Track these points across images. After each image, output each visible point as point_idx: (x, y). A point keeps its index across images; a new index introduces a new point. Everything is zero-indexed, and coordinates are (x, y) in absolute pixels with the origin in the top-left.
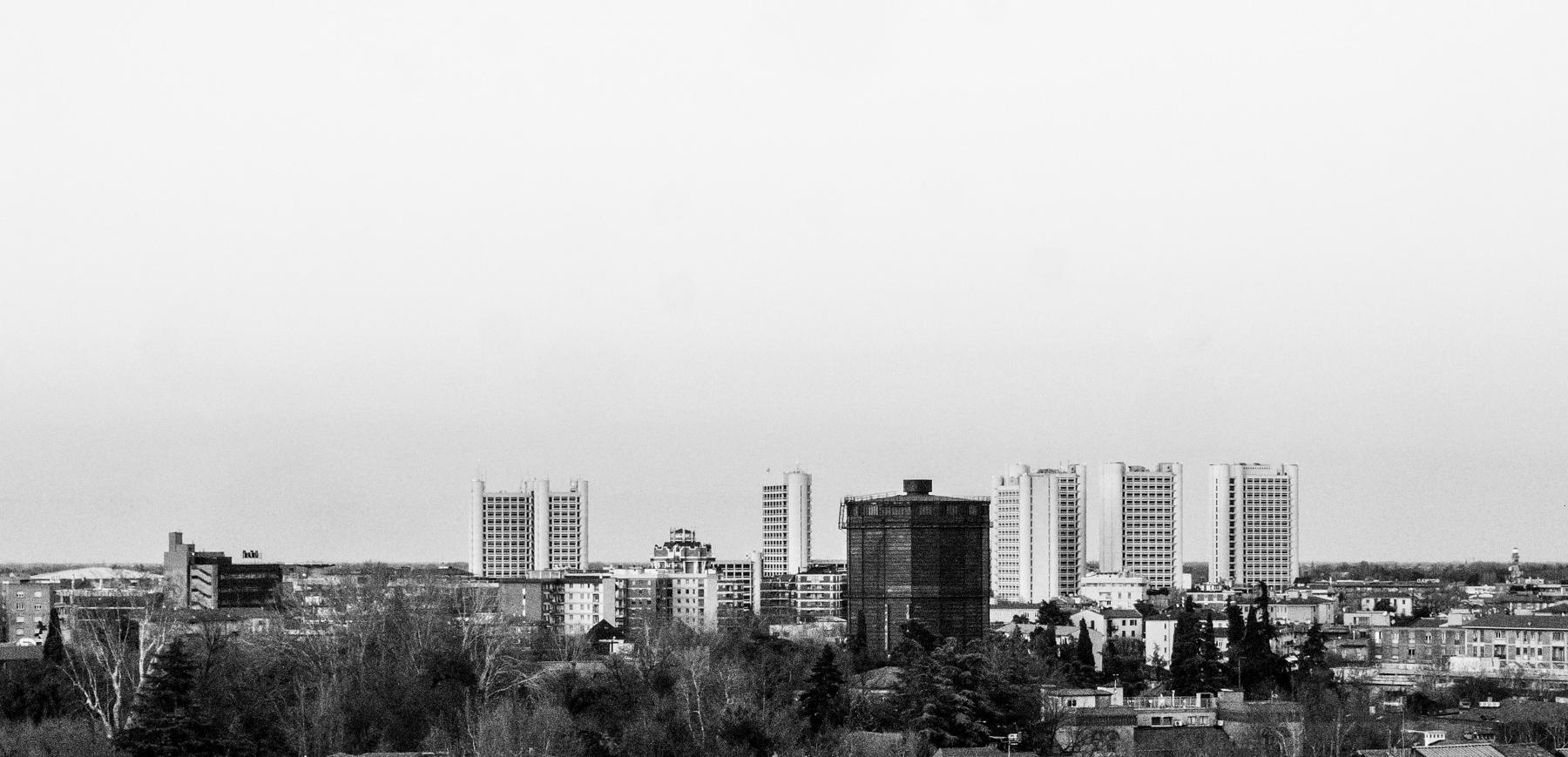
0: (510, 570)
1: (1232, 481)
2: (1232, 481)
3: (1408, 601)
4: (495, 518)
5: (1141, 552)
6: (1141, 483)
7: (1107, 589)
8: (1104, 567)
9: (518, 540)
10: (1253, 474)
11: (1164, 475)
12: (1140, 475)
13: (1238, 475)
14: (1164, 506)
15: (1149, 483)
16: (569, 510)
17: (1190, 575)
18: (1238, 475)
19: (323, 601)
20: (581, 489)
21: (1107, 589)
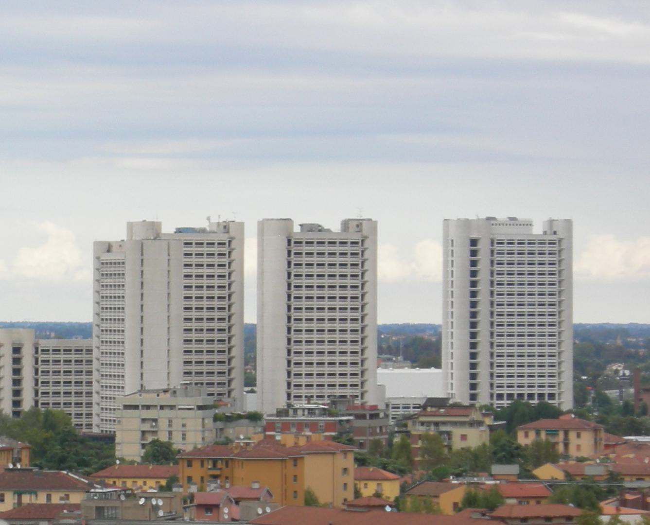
2: (474, 242)
10: (502, 233)
12: (315, 237)
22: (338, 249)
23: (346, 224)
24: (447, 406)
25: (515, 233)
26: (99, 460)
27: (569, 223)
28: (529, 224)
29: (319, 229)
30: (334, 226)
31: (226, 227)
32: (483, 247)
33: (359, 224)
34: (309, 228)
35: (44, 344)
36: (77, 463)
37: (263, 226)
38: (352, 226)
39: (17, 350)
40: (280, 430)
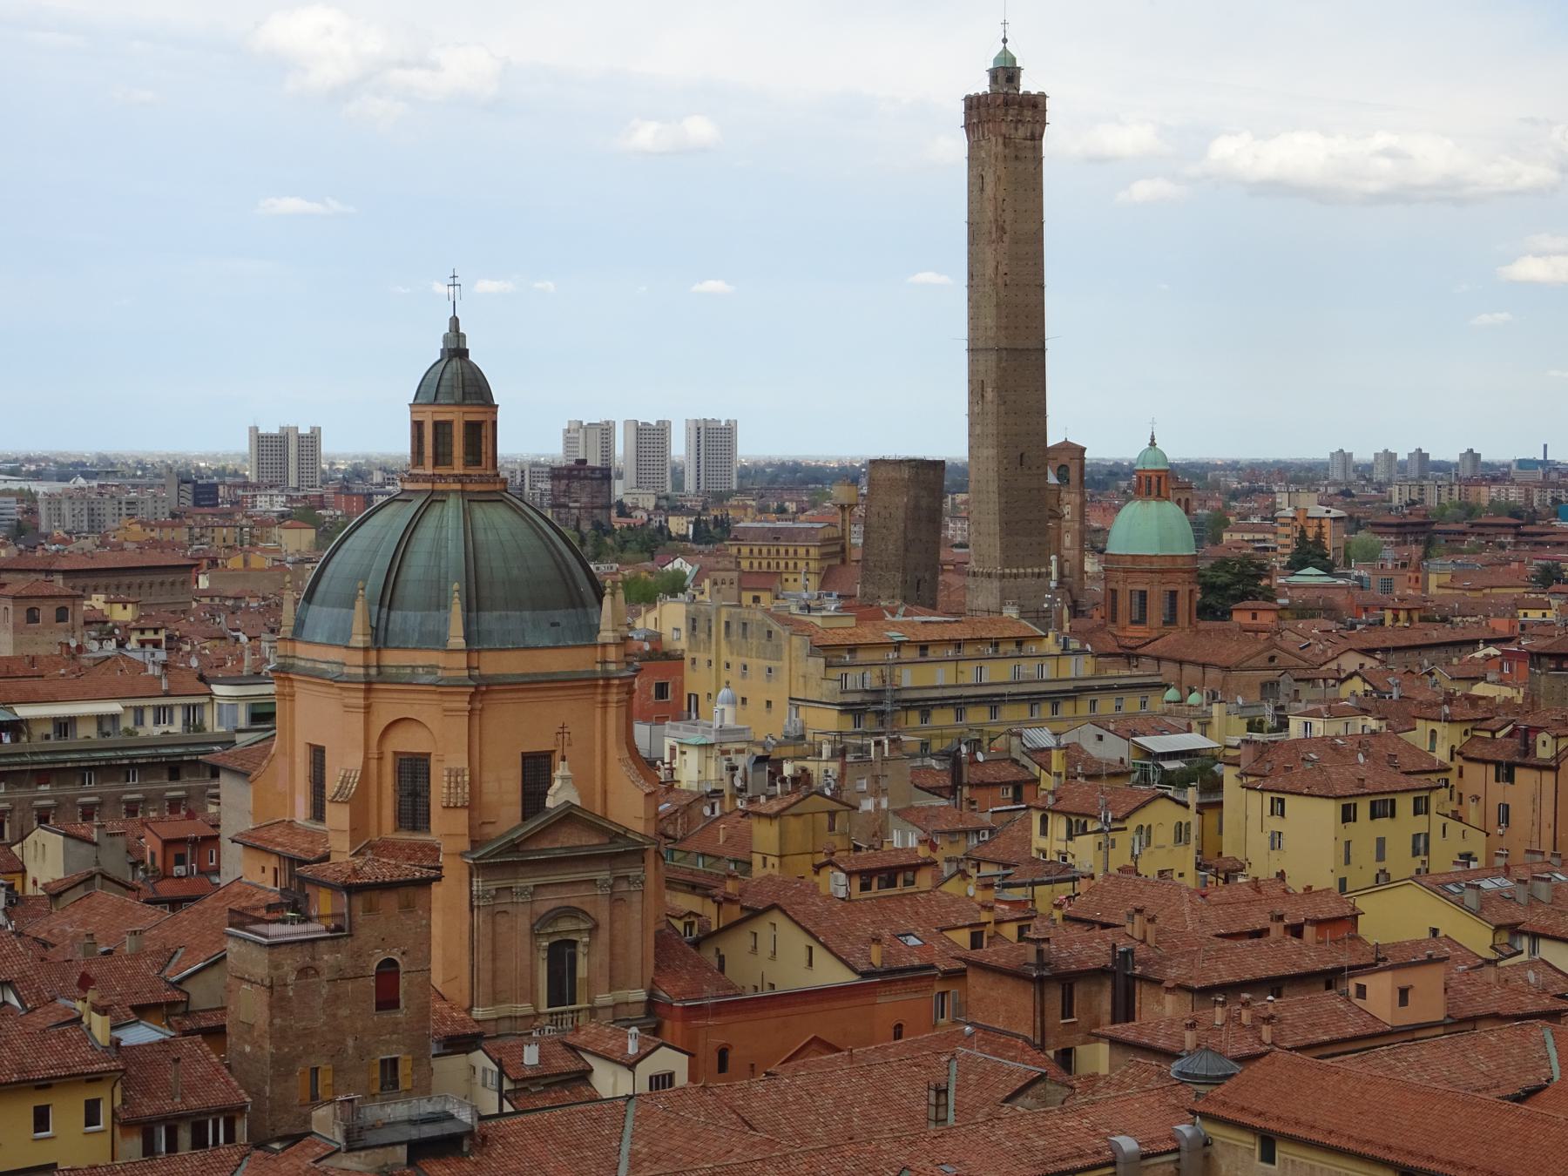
0: (274, 479)
1: (699, 429)
2: (699, 429)
3: (794, 504)
4: (265, 452)
5: (656, 467)
6: (647, 432)
7: (636, 496)
8: (528, 1058)
9: (278, 461)
10: (710, 426)
11: (661, 427)
12: (647, 427)
13: (702, 425)
14: (660, 450)
15: (652, 432)
16: (310, 453)
17: (536, 1062)
18: (702, 425)
19: (401, 1023)
20: (316, 432)
21: (636, 496)
22: (656, 432)
23: (658, 422)
24: (173, 877)
25: (715, 425)
26: (1206, 876)
27: (320, 428)
28: (720, 421)
29: (649, 424)
30: (654, 423)
31: (608, 423)
32: (702, 431)
33: (664, 422)
34: (643, 424)
35: (533, 469)
36: (257, 1148)
37: (626, 422)
38: (661, 423)
39: (523, 472)
40: (1480, 702)
